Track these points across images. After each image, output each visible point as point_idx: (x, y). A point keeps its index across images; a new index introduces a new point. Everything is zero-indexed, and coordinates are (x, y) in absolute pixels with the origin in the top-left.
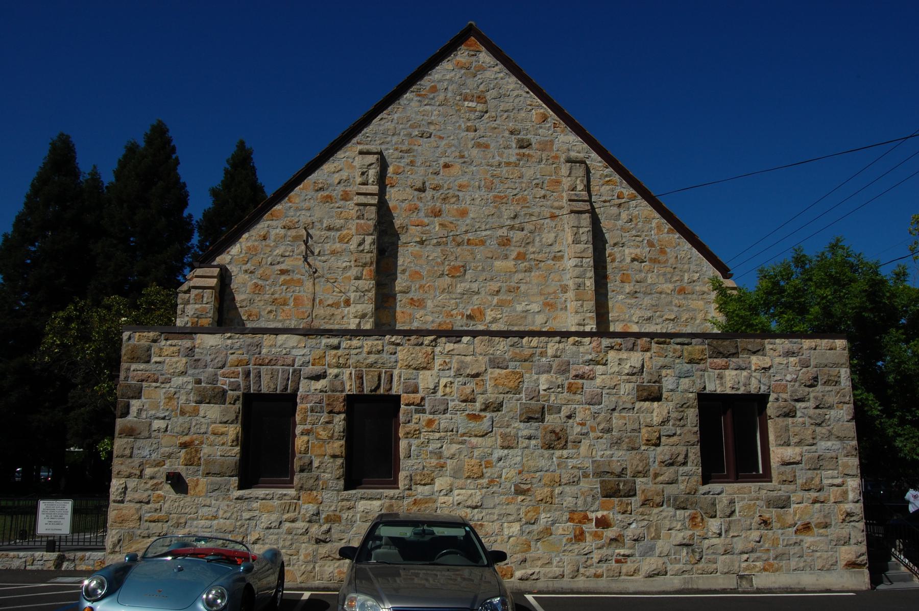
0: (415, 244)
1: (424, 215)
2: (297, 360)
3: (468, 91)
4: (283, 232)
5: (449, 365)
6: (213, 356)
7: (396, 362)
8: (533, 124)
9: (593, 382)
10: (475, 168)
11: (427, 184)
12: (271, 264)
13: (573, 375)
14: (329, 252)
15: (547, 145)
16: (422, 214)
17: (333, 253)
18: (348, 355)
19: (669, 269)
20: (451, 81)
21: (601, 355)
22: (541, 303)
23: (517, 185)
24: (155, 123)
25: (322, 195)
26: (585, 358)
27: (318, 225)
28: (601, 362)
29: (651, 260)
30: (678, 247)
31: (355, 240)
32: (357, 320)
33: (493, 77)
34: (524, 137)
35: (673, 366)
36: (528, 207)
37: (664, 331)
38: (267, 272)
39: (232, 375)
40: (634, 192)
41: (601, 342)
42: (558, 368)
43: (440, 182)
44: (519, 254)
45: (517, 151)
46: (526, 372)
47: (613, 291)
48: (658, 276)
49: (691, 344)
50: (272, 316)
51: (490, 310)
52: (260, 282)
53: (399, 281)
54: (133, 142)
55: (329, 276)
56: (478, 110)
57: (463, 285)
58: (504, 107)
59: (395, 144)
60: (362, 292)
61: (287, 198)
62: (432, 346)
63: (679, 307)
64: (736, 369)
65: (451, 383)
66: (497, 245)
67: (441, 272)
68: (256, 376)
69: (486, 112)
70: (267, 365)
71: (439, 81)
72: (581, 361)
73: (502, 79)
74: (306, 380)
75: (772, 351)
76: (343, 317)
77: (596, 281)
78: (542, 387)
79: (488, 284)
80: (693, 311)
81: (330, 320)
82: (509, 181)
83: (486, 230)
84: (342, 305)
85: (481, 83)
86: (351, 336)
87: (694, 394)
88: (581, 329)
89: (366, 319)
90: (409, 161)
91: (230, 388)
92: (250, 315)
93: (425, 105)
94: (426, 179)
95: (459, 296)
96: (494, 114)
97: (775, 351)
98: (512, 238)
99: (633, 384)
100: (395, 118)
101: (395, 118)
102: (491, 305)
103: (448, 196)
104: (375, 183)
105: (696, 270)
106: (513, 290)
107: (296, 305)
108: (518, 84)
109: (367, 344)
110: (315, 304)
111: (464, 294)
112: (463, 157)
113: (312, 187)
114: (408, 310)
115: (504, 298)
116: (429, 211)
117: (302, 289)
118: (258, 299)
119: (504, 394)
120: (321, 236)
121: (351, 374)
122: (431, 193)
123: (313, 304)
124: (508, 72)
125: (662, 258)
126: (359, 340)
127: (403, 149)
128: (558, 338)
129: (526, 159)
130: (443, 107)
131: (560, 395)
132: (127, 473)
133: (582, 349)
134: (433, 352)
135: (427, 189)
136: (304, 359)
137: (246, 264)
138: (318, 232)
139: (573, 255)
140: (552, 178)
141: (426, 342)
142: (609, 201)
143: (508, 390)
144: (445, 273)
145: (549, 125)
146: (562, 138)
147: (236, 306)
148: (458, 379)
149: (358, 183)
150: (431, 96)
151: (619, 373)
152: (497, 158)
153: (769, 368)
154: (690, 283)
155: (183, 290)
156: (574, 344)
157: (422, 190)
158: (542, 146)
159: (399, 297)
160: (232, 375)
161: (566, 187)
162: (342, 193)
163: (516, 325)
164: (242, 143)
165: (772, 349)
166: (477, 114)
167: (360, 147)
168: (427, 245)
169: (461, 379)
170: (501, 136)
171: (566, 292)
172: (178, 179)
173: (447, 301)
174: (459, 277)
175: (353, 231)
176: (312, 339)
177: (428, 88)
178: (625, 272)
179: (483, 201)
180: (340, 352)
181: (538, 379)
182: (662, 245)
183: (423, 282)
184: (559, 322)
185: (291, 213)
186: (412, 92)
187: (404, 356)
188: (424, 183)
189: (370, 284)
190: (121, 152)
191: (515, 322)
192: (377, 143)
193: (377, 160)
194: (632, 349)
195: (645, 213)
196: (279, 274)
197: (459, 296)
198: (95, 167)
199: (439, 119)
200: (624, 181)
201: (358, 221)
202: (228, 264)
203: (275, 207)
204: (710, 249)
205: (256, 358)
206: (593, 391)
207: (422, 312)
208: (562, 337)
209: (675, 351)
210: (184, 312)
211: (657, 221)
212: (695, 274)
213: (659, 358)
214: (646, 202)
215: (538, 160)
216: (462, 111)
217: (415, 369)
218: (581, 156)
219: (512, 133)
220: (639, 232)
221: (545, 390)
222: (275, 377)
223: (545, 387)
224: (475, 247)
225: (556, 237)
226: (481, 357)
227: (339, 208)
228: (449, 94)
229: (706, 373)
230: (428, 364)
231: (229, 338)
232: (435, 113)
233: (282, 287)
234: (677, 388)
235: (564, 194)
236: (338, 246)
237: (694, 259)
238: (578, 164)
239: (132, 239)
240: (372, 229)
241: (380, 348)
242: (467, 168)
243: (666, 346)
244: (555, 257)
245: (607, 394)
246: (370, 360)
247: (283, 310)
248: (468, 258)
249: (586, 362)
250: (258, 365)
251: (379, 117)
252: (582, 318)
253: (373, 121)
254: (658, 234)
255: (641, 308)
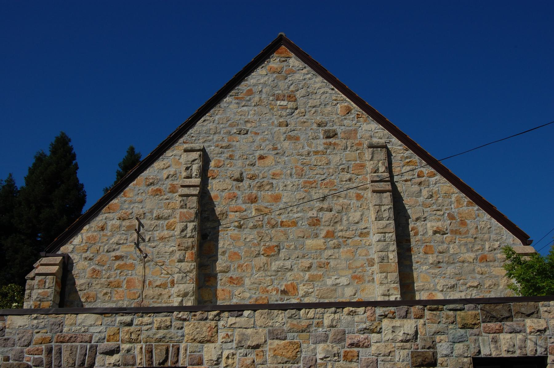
0: (234, 228)
1: (241, 202)
2: (94, 337)
3: (280, 92)
4: (118, 223)
5: (231, 338)
6: (20, 335)
7: (183, 336)
8: (338, 116)
9: (368, 350)
10: (287, 158)
11: (244, 174)
12: (108, 251)
13: (348, 344)
14: (158, 238)
15: (350, 134)
16: (240, 201)
17: (162, 239)
18: (139, 331)
19: (470, 239)
20: (265, 84)
21: (376, 324)
22: (350, 276)
23: (325, 171)
24: (59, 135)
25: (152, 189)
26: (359, 327)
27: (149, 215)
28: (375, 331)
29: (452, 231)
30: (478, 219)
31: (179, 227)
32: (180, 299)
33: (301, 78)
34: (331, 128)
35: (446, 331)
37: (469, 297)
39: (36, 352)
40: (433, 170)
41: (375, 311)
42: (334, 337)
43: (256, 172)
44: (328, 232)
45: (325, 141)
46: (304, 342)
47: (417, 262)
48: (459, 247)
49: (464, 309)
50: (107, 298)
51: (302, 285)
52: (98, 268)
53: (219, 261)
54: (41, 152)
55: (158, 260)
56: (289, 107)
57: (277, 263)
58: (312, 103)
59: (217, 141)
60: (185, 273)
61: (122, 193)
62: (216, 320)
63: (482, 274)
64: (511, 333)
65: (233, 355)
66: (308, 226)
67: (257, 252)
68: (57, 352)
69: (296, 109)
70: (67, 342)
71: (254, 85)
72: (356, 330)
73: (310, 79)
74: (101, 356)
75: (547, 313)
76: (170, 297)
77: (398, 254)
78: (319, 356)
79: (300, 261)
80: (495, 277)
81: (158, 299)
82: (318, 167)
83: (298, 212)
84: (169, 285)
85: (292, 84)
86: (143, 313)
87: (469, 358)
88: (386, 299)
89: (188, 297)
90: (228, 155)
91: (34, 364)
92: (88, 298)
93: (243, 106)
94: (243, 170)
95: (274, 273)
96: (303, 110)
97: (550, 313)
98: (322, 218)
99: (407, 350)
100: (217, 119)
101: (217, 119)
102: (303, 280)
103: (263, 184)
104: (198, 176)
105: (496, 239)
106: (323, 266)
107: (128, 287)
108: (324, 82)
109: (156, 320)
110: (145, 286)
111: (278, 271)
112: (276, 149)
113: (144, 182)
114: (228, 288)
115: (315, 273)
116: (247, 198)
117: (134, 272)
118: (96, 283)
119: (283, 363)
121: (141, 348)
122: (248, 182)
123: (144, 285)
124: (314, 72)
125: (463, 229)
126: (150, 316)
127: (223, 145)
128: (333, 309)
129: (332, 147)
130: (258, 107)
131: (337, 363)
133: (356, 318)
134: (217, 326)
135: (245, 179)
136: (100, 336)
137: (86, 252)
138: (149, 222)
139: (377, 231)
140: (357, 162)
141: (210, 317)
142: (410, 180)
143: (286, 360)
144: (261, 253)
145: (353, 116)
146: (365, 127)
147: (76, 289)
148: (240, 351)
149: (183, 177)
150: (248, 98)
151: (393, 340)
152: (307, 148)
153: (545, 330)
154: (492, 251)
155: (30, 276)
156: (349, 314)
157: (240, 180)
158: (347, 135)
159: (219, 276)
160: (36, 352)
161: (369, 171)
162: (169, 186)
163: (327, 298)
164: (132, 149)
165: (546, 311)
166: (288, 111)
167: (185, 146)
168: (244, 228)
169: (242, 350)
170: (310, 128)
171: (372, 266)
172: (78, 181)
173: (263, 278)
174: (274, 255)
175: (177, 220)
176: (108, 317)
177: (244, 92)
178: (428, 244)
179: (295, 187)
180: (132, 328)
181: (315, 348)
182: (462, 217)
183: (242, 262)
184: (367, 294)
185: (126, 206)
186: (231, 96)
187: (190, 331)
188: (241, 174)
189: (191, 265)
190: (31, 162)
191: (325, 295)
192: (200, 141)
193: (200, 156)
194: (405, 317)
195: (444, 189)
196: (115, 260)
197: (274, 273)
198: (11, 175)
199: (255, 117)
200: (423, 161)
201: (182, 210)
202: (71, 253)
203: (112, 202)
204: (508, 218)
205: (58, 336)
206: (368, 359)
207: (240, 289)
208: (337, 308)
209: (448, 317)
210: (30, 296)
211: (456, 195)
212: (496, 243)
213: (432, 324)
214: (445, 179)
215: (343, 148)
216: (275, 109)
217: (200, 342)
218: (382, 141)
219: (319, 125)
220: (439, 206)
221: (322, 359)
222: (74, 353)
223: (322, 356)
224: (288, 228)
225: (362, 215)
226: (261, 330)
227: (166, 199)
228: (264, 96)
229: (480, 338)
230: (212, 337)
231: (36, 318)
232: (251, 112)
233: (117, 271)
234: (452, 353)
235: (368, 176)
236: (166, 233)
237: (493, 228)
238: (379, 149)
239: (39, 235)
240: (193, 217)
241: (168, 323)
242: (280, 158)
243: (439, 312)
244: (361, 233)
245: (382, 361)
246: (159, 335)
247: (117, 292)
248: (282, 238)
249: (361, 331)
250: (59, 342)
251: (203, 119)
252: (387, 289)
253: (198, 123)
254: (457, 207)
255: (445, 277)
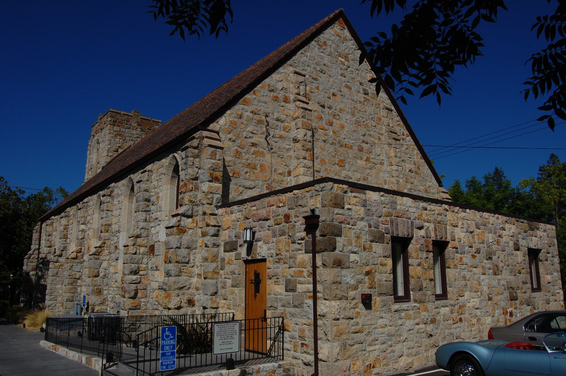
12: (245, 137)
17: (281, 137)
36: (369, 130)
38: (243, 143)
52: (239, 150)
60: (307, 168)
61: (253, 91)
93: (321, 52)
107: (262, 170)
112: (341, 91)
113: (267, 87)
120: (273, 124)
132: (340, 296)
137: (230, 134)
251: (300, 52)
